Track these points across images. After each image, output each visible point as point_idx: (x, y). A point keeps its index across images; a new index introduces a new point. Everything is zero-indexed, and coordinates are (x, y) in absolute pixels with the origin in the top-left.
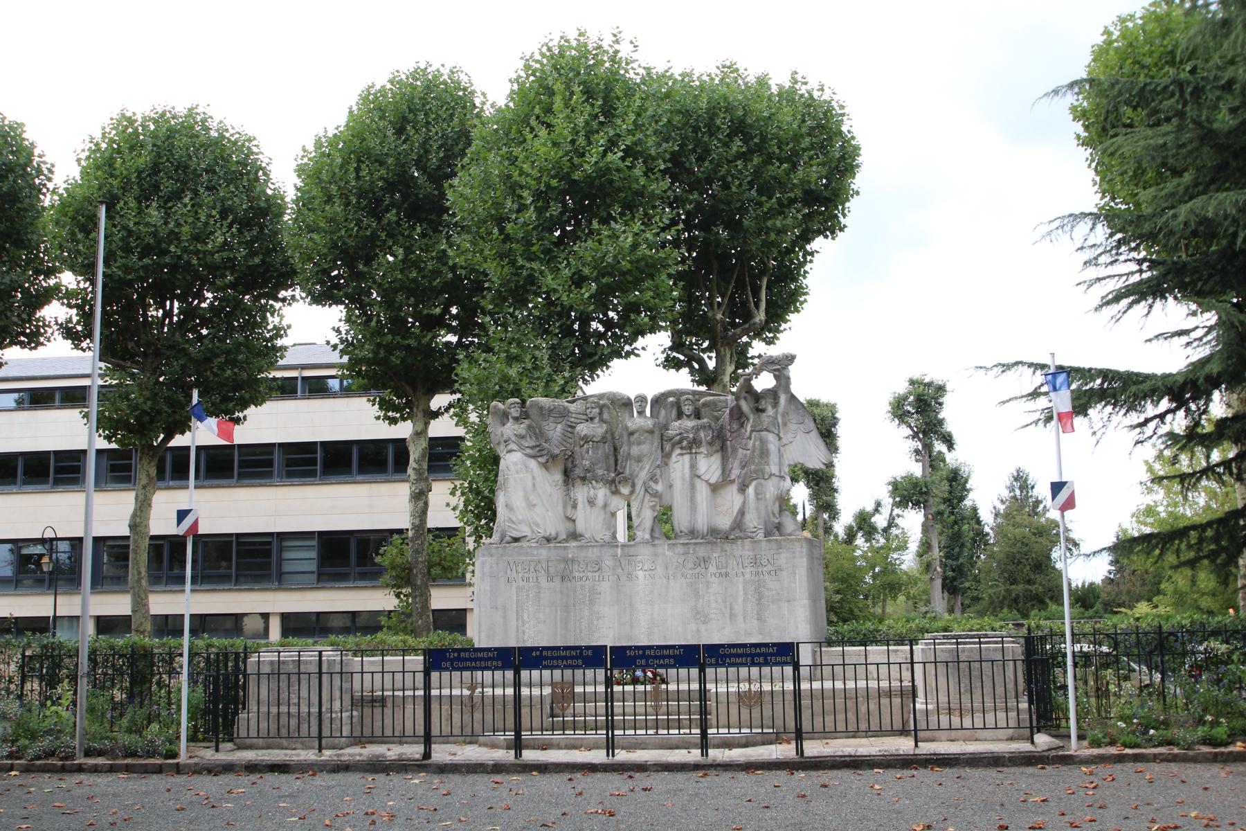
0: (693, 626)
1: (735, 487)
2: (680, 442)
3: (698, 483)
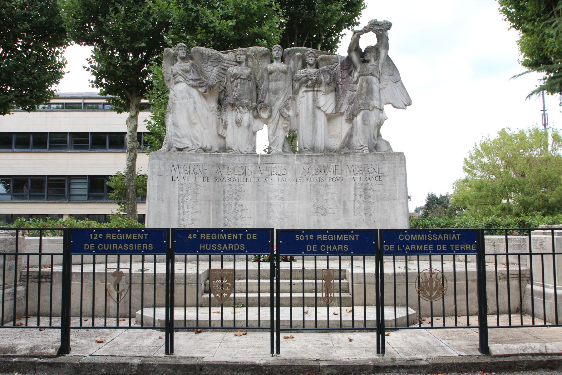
0: (315, 218)
1: (344, 118)
2: (306, 82)
3: (318, 112)
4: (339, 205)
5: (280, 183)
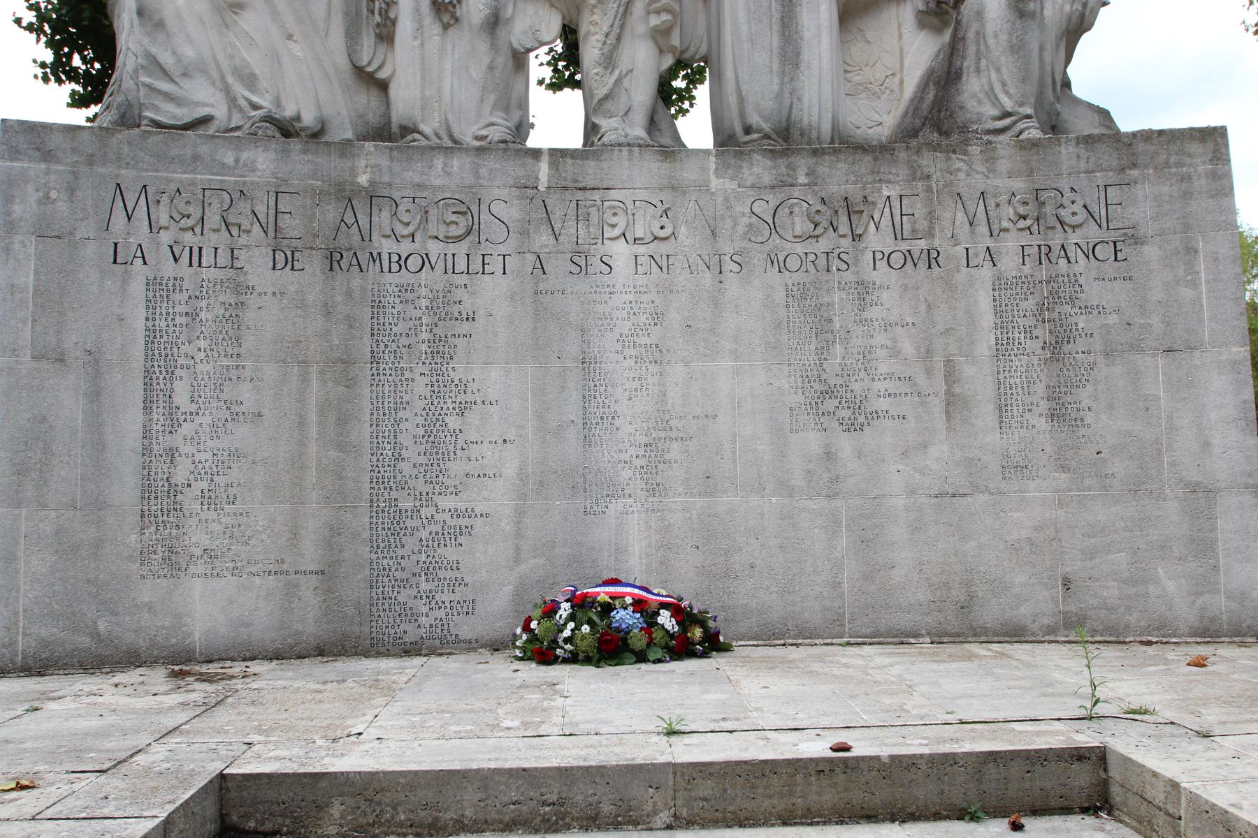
4: (921, 379)
5: (641, 280)
